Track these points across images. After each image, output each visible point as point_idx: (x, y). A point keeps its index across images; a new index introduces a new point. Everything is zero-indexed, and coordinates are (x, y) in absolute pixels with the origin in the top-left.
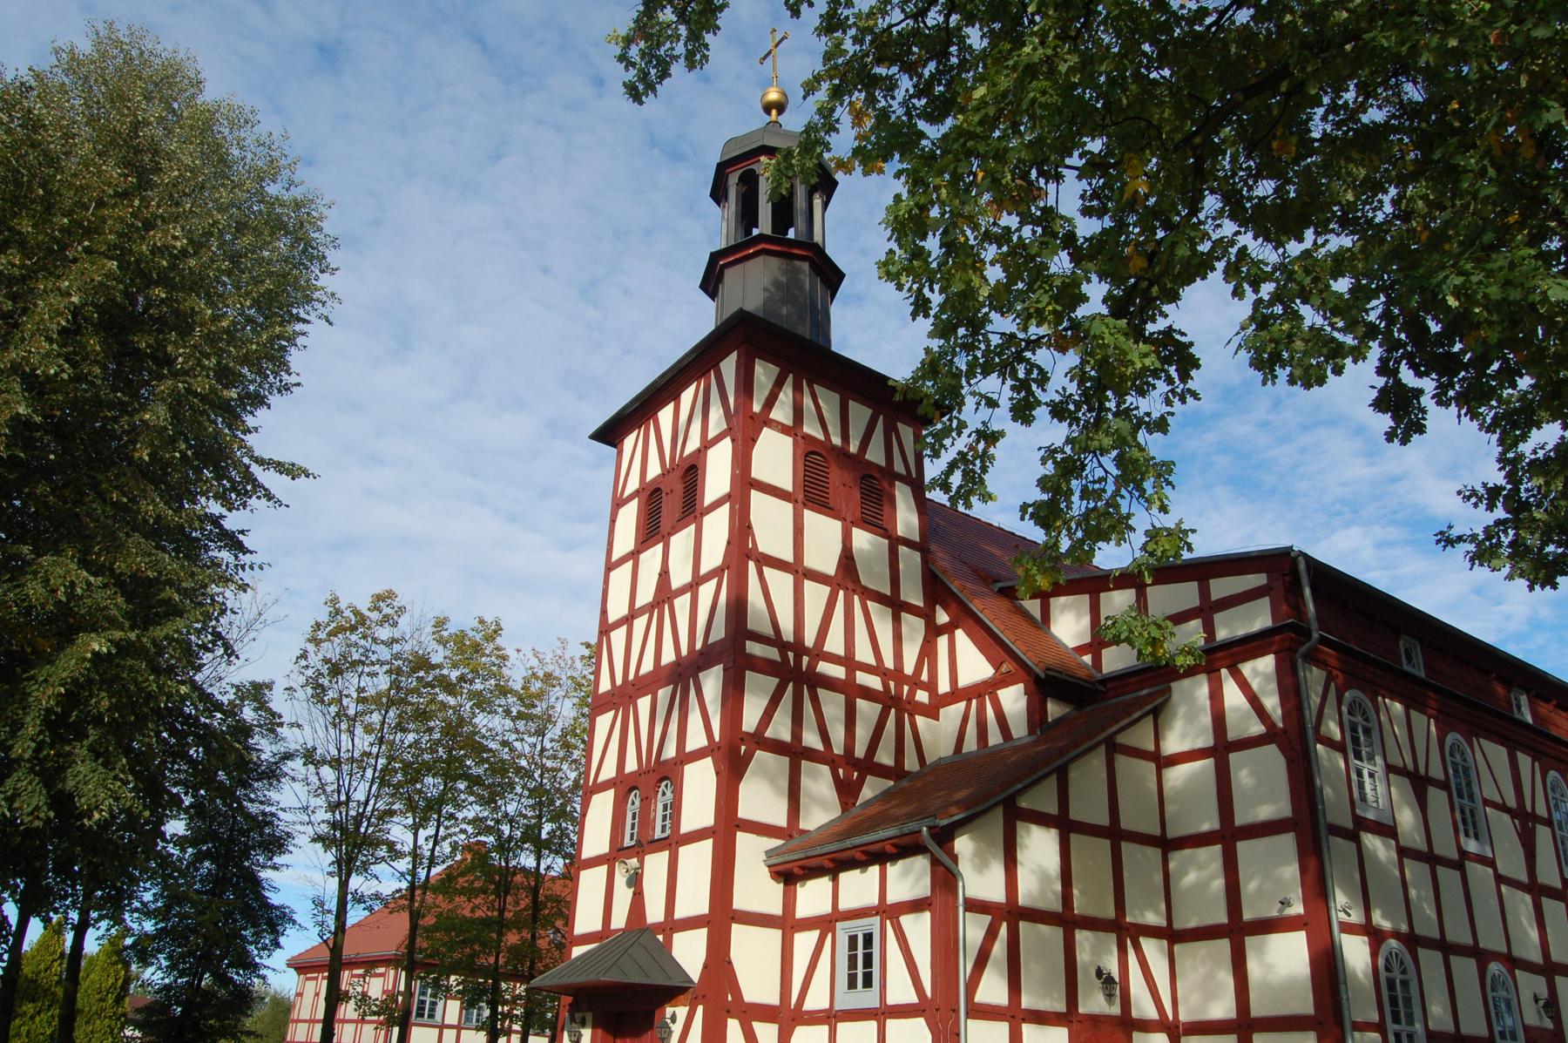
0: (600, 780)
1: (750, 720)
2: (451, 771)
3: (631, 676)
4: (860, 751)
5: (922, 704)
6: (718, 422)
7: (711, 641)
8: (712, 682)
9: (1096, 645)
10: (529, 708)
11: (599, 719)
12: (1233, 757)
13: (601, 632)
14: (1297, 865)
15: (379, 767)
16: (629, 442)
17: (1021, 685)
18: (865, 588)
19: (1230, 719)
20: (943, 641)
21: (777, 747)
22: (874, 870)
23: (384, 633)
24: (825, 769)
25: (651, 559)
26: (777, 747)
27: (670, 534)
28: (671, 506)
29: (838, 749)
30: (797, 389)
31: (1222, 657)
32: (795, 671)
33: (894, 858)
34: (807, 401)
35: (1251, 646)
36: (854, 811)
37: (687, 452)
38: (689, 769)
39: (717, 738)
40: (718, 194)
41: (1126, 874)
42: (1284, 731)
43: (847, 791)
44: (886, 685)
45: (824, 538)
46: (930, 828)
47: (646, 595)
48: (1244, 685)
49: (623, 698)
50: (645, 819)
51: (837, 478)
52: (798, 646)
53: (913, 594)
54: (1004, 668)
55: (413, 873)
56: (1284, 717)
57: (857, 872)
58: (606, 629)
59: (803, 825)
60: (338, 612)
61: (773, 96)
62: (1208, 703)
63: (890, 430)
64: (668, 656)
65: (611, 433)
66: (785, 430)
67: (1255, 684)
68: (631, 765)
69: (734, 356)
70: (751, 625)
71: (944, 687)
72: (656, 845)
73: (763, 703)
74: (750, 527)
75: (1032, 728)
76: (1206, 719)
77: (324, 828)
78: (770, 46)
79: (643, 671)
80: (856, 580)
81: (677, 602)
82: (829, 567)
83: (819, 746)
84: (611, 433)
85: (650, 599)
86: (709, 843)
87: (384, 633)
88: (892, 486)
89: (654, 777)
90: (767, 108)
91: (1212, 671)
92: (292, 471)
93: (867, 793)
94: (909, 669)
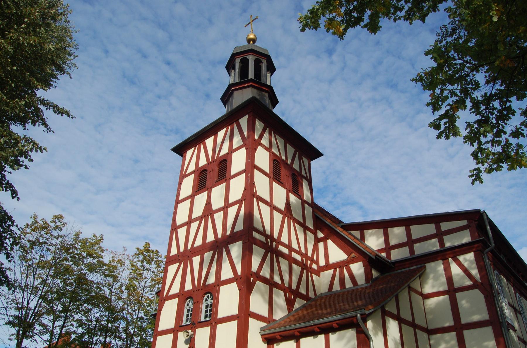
0: (170, 294)
1: (255, 267)
2: (74, 297)
3: (189, 248)
4: (294, 287)
5: (314, 269)
6: (238, 142)
7: (235, 230)
8: (236, 249)
9: (388, 248)
10: (110, 272)
11: (170, 267)
12: (458, 295)
13: (172, 230)
14: (495, 342)
15: (44, 290)
16: (189, 153)
17: (361, 263)
18: (294, 218)
19: (455, 279)
20: (321, 245)
21: (264, 280)
22: (322, 337)
23: (55, 233)
24: (282, 293)
25: (201, 199)
26: (264, 280)
27: (211, 188)
28: (211, 177)
29: (287, 285)
30: (270, 134)
31: (445, 254)
32: (271, 248)
33: (334, 330)
34: (273, 140)
35: (463, 249)
36: (293, 313)
37: (222, 154)
38: (223, 289)
39: (239, 273)
40: (230, 67)
41: (419, 344)
42: (482, 284)
43: (290, 303)
44: (302, 260)
45: (280, 196)
46: (361, 315)
47: (198, 211)
48: (460, 265)
49: (184, 257)
50: (195, 312)
51: (284, 172)
52: (271, 237)
53: (310, 225)
54: (353, 255)
55: (51, 340)
56: (481, 278)
57: (311, 338)
58: (175, 228)
59: (274, 318)
60: (36, 222)
61: (252, 36)
62: (444, 272)
63: (300, 159)
64: (210, 238)
65: (180, 150)
66: (266, 148)
67: (466, 264)
68: (188, 287)
69: (247, 117)
70: (255, 225)
71: (322, 263)
72: (203, 324)
73: (260, 260)
74: (254, 184)
75: (367, 281)
76: (444, 279)
77: (11, 319)
78: (250, 21)
79: (196, 245)
80: (291, 214)
81: (216, 215)
82: (282, 207)
83: (280, 282)
84: (180, 150)
85: (200, 214)
86: (235, 322)
87: (55, 233)
88: (302, 180)
89: (202, 292)
90: (249, 41)
91: (445, 259)
92: (60, 111)
93: (297, 306)
94: (310, 254)
